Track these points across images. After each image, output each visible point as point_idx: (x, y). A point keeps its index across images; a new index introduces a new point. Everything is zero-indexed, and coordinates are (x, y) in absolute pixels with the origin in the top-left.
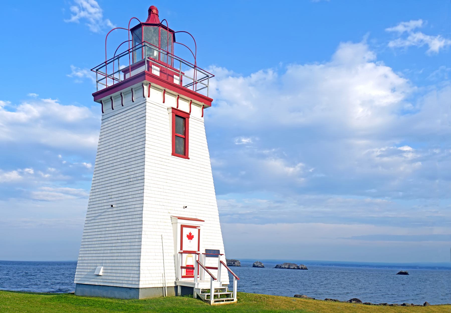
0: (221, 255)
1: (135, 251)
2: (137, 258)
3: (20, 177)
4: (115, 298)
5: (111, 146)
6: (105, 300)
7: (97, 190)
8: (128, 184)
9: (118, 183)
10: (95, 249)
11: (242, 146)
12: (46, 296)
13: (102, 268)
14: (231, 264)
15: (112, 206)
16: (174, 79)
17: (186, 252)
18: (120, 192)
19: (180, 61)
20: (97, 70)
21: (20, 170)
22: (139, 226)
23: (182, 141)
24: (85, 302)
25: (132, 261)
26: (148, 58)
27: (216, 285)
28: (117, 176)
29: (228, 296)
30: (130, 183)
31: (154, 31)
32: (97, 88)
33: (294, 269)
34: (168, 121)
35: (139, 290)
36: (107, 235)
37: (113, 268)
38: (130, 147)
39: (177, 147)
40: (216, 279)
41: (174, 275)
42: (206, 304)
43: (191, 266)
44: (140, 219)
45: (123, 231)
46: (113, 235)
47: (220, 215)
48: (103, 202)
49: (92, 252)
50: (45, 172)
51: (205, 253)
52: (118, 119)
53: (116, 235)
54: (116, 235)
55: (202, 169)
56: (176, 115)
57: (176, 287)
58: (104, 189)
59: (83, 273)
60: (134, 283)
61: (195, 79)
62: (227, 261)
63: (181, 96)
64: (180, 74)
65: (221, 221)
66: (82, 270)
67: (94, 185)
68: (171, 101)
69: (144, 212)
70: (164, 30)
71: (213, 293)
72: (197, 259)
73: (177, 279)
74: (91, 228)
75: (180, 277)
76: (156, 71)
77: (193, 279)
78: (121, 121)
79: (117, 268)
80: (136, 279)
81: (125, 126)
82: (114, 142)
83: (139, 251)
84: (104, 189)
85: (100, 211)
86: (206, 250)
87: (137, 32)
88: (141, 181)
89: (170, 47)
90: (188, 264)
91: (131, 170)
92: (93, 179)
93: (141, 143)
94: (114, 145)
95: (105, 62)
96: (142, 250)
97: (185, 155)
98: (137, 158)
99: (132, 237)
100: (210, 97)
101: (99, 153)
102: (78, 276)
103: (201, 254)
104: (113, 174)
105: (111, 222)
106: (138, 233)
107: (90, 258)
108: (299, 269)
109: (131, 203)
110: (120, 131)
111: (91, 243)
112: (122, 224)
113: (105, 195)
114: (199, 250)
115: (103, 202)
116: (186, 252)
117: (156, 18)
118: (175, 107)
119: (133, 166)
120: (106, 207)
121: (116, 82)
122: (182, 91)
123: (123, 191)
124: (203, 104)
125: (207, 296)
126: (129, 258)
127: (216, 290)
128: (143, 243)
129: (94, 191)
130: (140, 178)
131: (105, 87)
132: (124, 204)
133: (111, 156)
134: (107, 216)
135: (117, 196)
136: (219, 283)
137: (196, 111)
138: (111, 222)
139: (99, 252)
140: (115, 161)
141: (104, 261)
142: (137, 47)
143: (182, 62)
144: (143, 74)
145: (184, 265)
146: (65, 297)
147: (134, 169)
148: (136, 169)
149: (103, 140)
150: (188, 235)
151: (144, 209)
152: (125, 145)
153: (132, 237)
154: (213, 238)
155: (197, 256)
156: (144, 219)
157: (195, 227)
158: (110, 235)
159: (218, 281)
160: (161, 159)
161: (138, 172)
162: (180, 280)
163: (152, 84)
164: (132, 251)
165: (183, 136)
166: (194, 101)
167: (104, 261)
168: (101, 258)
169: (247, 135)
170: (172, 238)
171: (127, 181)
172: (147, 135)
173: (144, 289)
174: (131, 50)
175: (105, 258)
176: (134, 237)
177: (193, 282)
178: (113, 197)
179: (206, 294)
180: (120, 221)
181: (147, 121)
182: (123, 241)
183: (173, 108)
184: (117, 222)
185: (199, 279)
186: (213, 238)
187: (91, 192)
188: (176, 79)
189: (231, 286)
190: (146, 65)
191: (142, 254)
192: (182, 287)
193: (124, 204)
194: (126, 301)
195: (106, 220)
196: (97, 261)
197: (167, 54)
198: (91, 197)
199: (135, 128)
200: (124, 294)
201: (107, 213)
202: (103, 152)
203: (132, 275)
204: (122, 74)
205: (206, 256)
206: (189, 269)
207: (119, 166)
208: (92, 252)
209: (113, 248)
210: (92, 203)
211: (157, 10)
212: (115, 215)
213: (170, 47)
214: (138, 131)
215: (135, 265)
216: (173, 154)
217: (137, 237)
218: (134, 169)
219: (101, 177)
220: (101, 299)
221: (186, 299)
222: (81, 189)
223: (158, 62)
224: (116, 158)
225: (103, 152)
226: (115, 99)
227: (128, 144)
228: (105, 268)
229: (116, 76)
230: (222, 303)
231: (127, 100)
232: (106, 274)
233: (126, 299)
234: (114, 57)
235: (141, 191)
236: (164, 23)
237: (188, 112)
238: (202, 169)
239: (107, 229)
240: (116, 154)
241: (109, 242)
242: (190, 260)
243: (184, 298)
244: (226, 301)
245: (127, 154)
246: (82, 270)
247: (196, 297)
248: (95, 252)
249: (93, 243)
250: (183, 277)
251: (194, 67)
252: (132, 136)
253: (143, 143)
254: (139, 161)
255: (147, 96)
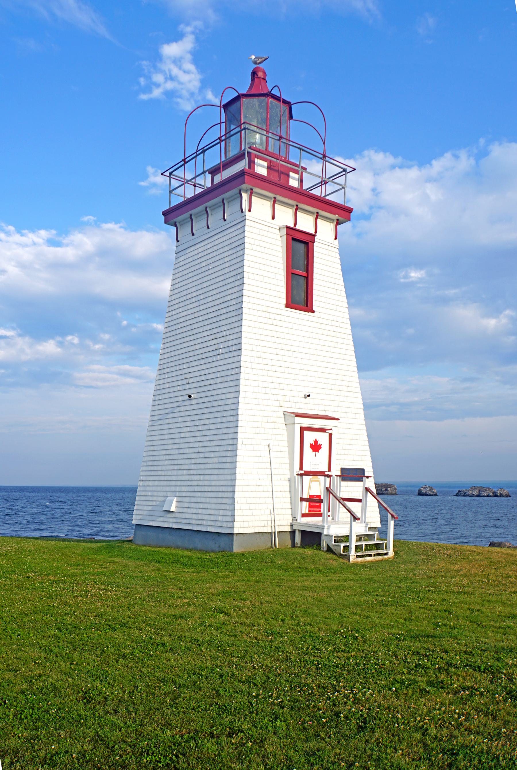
0: (368, 477)
1: (226, 471)
2: (229, 483)
3: (59, 350)
4: (195, 549)
5: (189, 297)
6: (180, 552)
7: (167, 370)
8: (214, 359)
9: (199, 357)
10: (164, 468)
11: (411, 285)
12: (89, 545)
13: (175, 499)
14: (382, 490)
15: (190, 396)
16: (290, 180)
17: (308, 473)
18: (203, 372)
19: (299, 148)
20: (171, 174)
21: (59, 339)
22: (232, 430)
23: (302, 281)
24: (149, 555)
25: (221, 489)
26: (250, 148)
27: (359, 528)
28: (198, 346)
29: (378, 546)
30: (219, 357)
31: (259, 105)
32: (170, 202)
33: (488, 496)
34: (280, 249)
35: (233, 537)
36: (183, 446)
37: (193, 500)
38: (218, 296)
39: (295, 292)
40: (359, 519)
41: (289, 512)
42: (342, 560)
43: (317, 496)
44: (234, 419)
45: (208, 438)
46: (191, 445)
47: (367, 407)
48: (175, 389)
49: (159, 473)
50: (96, 341)
51: (339, 474)
52: (200, 250)
53: (197, 445)
54: (197, 445)
55: (335, 329)
56: (293, 239)
57: (293, 532)
58: (178, 368)
59: (145, 508)
60: (224, 525)
61: (324, 176)
62: (377, 486)
63: (301, 205)
64: (300, 169)
65: (367, 417)
66: (144, 503)
67: (162, 362)
68: (285, 216)
69: (240, 406)
70: (275, 102)
71: (354, 543)
72: (328, 486)
73: (294, 519)
74: (157, 433)
75: (300, 515)
76: (261, 168)
77: (320, 519)
78: (205, 253)
79: (199, 500)
80: (229, 519)
81: (212, 261)
82: (194, 289)
83: (232, 471)
84: (178, 368)
85: (171, 405)
86: (342, 470)
87: (233, 108)
88: (236, 353)
89: (284, 127)
90: (312, 494)
91: (221, 335)
92: (161, 352)
93: (236, 289)
94: (194, 294)
95: (184, 160)
96: (238, 471)
97: (307, 306)
98: (229, 315)
99: (222, 448)
100: (349, 205)
101: (171, 309)
102: (138, 512)
103: (334, 475)
104: (191, 343)
105: (188, 424)
106: (231, 442)
107: (156, 483)
108: (496, 496)
109: (220, 391)
110: (203, 269)
111: (157, 458)
112: (206, 427)
113: (180, 378)
114: (330, 470)
115: (175, 389)
116: (308, 473)
117: (263, 84)
118: (292, 225)
119: (223, 328)
120: (180, 399)
121: (199, 190)
122: (303, 198)
123: (207, 372)
124: (336, 217)
125: (344, 547)
126: (218, 483)
127: (359, 538)
128: (239, 458)
129: (162, 372)
130: (234, 348)
131: (182, 200)
132: (210, 393)
133: (189, 312)
134: (182, 414)
135: (198, 379)
136: (364, 525)
137: (325, 231)
138: (188, 424)
139: (169, 473)
140: (195, 321)
141: (178, 489)
142: (232, 133)
143: (304, 150)
144: (242, 174)
145: (306, 496)
146: (118, 547)
147: (224, 334)
148: (228, 332)
149: (177, 286)
150: (311, 445)
151: (241, 400)
152: (210, 293)
153: (222, 448)
154: (353, 448)
155: (328, 479)
156: (240, 418)
157: (324, 430)
158: (187, 445)
159: (361, 523)
160: (268, 315)
161: (231, 337)
162: (299, 521)
163: (256, 190)
164: (221, 472)
165: (305, 274)
166: (322, 213)
167: (178, 489)
168: (173, 483)
169: (419, 265)
170: (286, 449)
171: (214, 353)
172: (245, 275)
173: (242, 536)
174: (223, 138)
175: (179, 483)
176: (225, 448)
177: (321, 524)
178: (191, 381)
179: (342, 545)
180: (202, 422)
181: (246, 251)
182: (207, 455)
183: (287, 227)
184: (197, 423)
185: (330, 519)
186: (353, 448)
187: (159, 373)
188: (294, 178)
189: (383, 532)
190: (247, 159)
191: (238, 477)
192: (303, 532)
193: (210, 393)
194: (214, 556)
195: (180, 419)
196: (167, 489)
197: (279, 140)
198: (158, 383)
199: (227, 265)
200: (211, 544)
201: (182, 409)
202: (176, 306)
203: (221, 512)
204: (209, 176)
205: (343, 480)
206: (314, 502)
207: (201, 329)
208: (159, 473)
209: (192, 467)
210: (158, 392)
211: (264, 73)
212: (195, 412)
213: (284, 127)
214: (232, 268)
215: (225, 501)
216: (287, 306)
217: (230, 448)
218: (224, 334)
219: (173, 348)
220: (174, 552)
221: (310, 552)
222: (147, 368)
223: (265, 154)
224: (196, 315)
225: (176, 306)
226: (196, 218)
227: (215, 292)
228: (180, 499)
229: (199, 180)
230: (368, 559)
231: (215, 218)
232: (181, 510)
233: (213, 551)
234: (197, 151)
235: (236, 371)
236: (275, 92)
237: (313, 232)
238: (335, 329)
239: (183, 435)
240: (197, 309)
241: (185, 456)
242: (315, 487)
243: (306, 550)
244: (375, 555)
245: (214, 309)
246: (144, 503)
247: (325, 549)
248: (163, 473)
249: (162, 458)
250: (304, 515)
251: (321, 156)
252: (221, 278)
253: (240, 288)
254: (234, 319)
255: (247, 209)
